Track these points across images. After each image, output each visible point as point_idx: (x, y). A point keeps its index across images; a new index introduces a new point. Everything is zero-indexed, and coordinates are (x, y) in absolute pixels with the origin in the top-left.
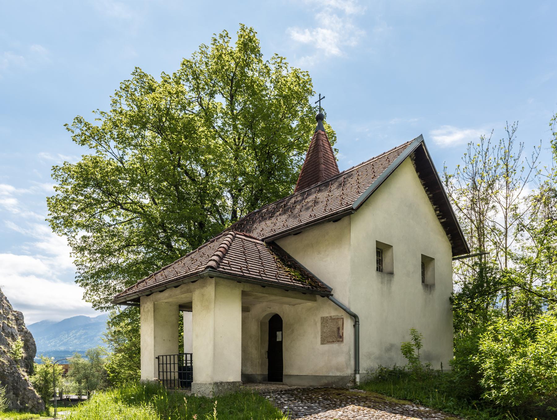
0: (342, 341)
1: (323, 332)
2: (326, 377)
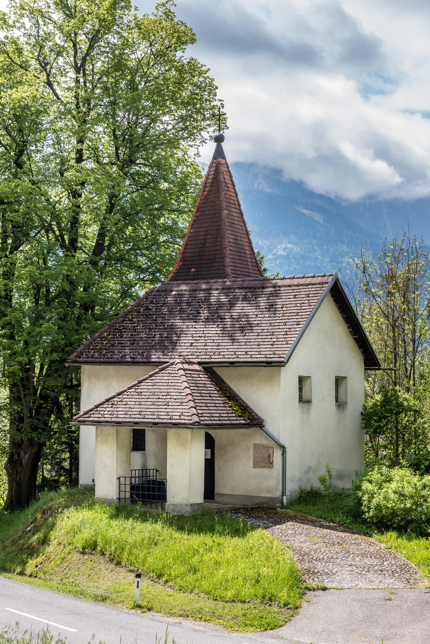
0: (272, 467)
1: (255, 457)
2: (258, 497)
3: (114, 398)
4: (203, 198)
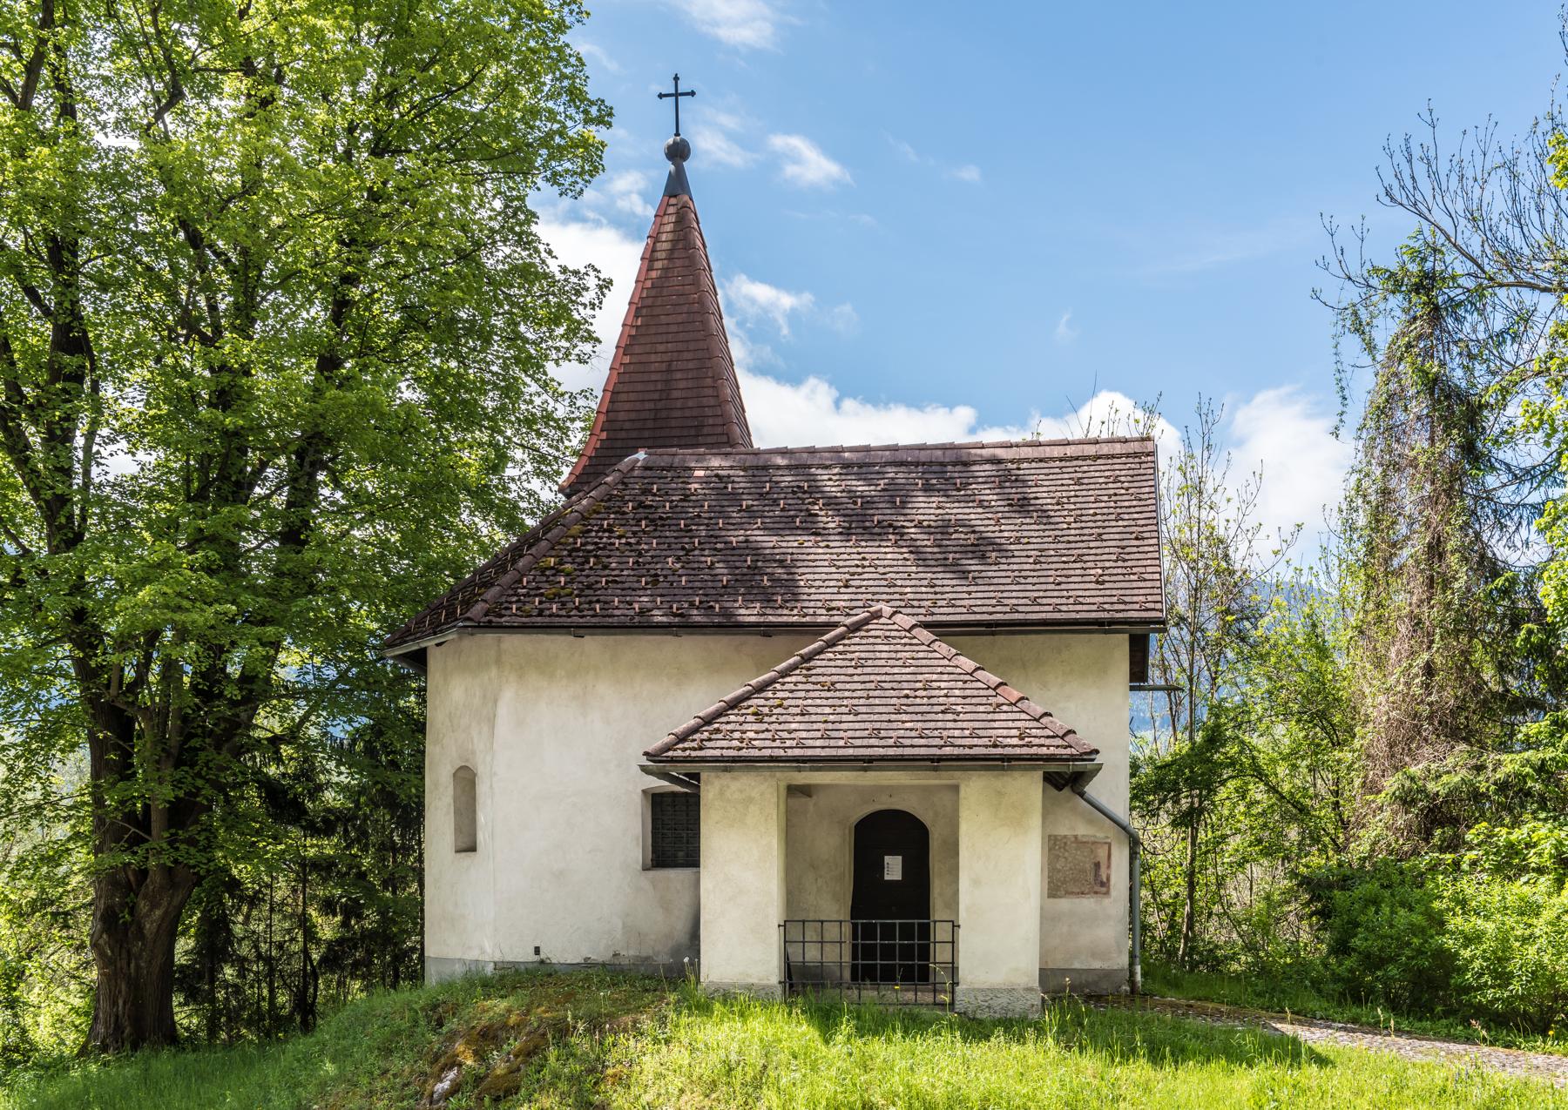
0: (1107, 893)
3: (749, 698)
4: (649, 284)
